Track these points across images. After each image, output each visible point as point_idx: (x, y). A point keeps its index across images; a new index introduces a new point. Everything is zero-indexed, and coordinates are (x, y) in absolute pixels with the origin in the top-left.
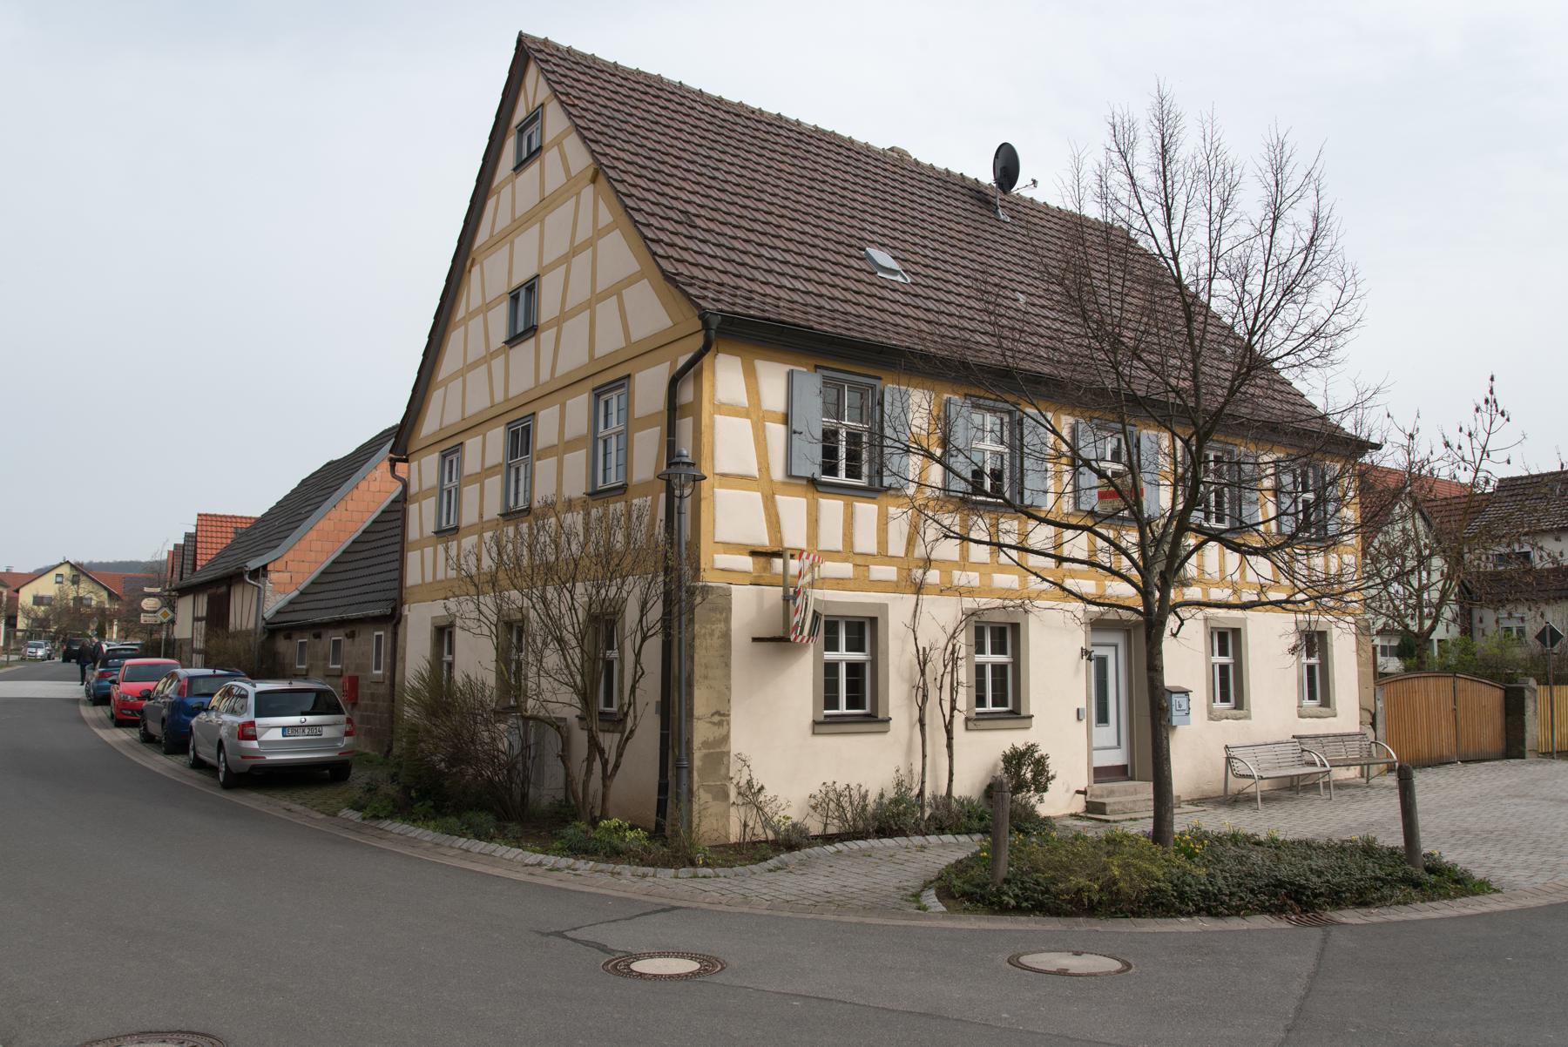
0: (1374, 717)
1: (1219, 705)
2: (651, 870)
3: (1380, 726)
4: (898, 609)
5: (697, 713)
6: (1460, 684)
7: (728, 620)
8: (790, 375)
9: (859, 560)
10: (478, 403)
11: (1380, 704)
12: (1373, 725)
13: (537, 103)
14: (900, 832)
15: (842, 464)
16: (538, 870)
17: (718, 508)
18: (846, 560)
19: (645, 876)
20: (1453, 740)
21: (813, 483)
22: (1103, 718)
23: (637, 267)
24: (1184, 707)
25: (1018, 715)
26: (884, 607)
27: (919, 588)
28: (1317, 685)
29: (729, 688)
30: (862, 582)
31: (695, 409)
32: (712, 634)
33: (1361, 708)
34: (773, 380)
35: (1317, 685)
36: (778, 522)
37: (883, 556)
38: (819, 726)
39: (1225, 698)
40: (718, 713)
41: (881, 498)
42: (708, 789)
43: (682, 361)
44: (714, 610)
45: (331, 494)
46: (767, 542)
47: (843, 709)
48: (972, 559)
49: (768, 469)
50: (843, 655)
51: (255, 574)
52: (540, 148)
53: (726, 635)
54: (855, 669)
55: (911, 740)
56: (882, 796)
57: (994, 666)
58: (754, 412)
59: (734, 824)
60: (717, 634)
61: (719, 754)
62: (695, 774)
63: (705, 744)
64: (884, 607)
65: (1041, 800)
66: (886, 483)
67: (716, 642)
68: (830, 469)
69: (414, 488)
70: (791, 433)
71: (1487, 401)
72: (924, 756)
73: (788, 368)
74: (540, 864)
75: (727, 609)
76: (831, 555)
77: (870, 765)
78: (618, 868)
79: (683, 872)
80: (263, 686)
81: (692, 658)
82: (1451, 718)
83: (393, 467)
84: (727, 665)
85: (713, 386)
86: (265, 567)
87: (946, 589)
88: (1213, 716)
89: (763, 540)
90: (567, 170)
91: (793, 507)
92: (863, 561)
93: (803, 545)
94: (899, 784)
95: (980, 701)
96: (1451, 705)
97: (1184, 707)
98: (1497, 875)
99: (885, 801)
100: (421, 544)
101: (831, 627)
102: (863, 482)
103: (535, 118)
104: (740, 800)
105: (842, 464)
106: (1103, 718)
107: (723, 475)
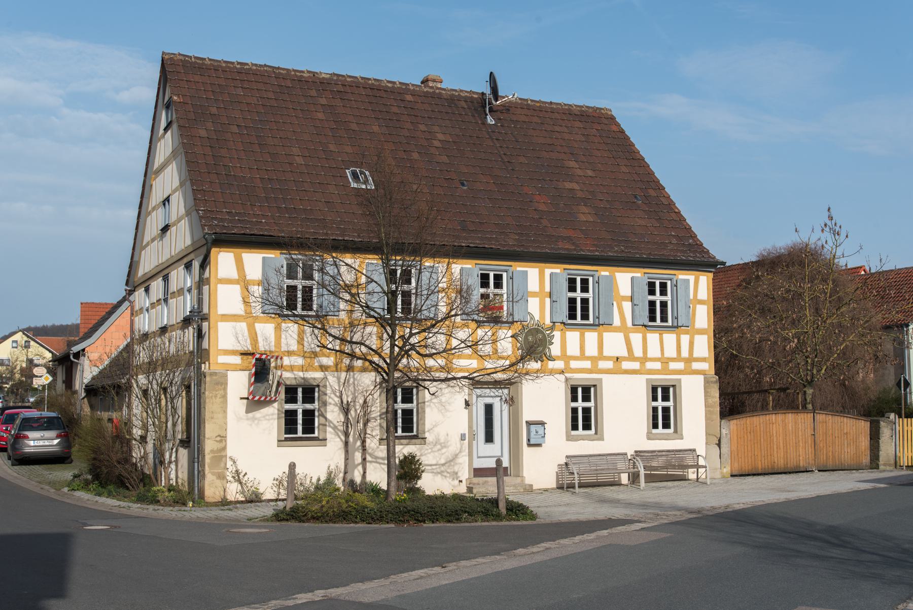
0: (719, 441)
4: (332, 381)
7: (225, 389)
8: (264, 258)
11: (724, 431)
12: (719, 445)
20: (810, 450)
22: (489, 438)
24: (541, 432)
25: (418, 438)
26: (601, 380)
27: (350, 369)
28: (663, 418)
29: (226, 424)
30: (665, 370)
31: (208, 281)
32: (216, 397)
33: (707, 434)
34: (254, 262)
35: (663, 418)
37: (583, 357)
40: (219, 436)
42: (213, 474)
51: (77, 355)
56: (319, 480)
57: (404, 411)
58: (244, 283)
61: (220, 455)
63: (212, 451)
64: (601, 380)
76: (673, 360)
77: (318, 462)
84: (225, 412)
86: (83, 350)
89: (250, 348)
91: (266, 330)
92: (665, 361)
94: (330, 474)
96: (810, 432)
106: (489, 438)
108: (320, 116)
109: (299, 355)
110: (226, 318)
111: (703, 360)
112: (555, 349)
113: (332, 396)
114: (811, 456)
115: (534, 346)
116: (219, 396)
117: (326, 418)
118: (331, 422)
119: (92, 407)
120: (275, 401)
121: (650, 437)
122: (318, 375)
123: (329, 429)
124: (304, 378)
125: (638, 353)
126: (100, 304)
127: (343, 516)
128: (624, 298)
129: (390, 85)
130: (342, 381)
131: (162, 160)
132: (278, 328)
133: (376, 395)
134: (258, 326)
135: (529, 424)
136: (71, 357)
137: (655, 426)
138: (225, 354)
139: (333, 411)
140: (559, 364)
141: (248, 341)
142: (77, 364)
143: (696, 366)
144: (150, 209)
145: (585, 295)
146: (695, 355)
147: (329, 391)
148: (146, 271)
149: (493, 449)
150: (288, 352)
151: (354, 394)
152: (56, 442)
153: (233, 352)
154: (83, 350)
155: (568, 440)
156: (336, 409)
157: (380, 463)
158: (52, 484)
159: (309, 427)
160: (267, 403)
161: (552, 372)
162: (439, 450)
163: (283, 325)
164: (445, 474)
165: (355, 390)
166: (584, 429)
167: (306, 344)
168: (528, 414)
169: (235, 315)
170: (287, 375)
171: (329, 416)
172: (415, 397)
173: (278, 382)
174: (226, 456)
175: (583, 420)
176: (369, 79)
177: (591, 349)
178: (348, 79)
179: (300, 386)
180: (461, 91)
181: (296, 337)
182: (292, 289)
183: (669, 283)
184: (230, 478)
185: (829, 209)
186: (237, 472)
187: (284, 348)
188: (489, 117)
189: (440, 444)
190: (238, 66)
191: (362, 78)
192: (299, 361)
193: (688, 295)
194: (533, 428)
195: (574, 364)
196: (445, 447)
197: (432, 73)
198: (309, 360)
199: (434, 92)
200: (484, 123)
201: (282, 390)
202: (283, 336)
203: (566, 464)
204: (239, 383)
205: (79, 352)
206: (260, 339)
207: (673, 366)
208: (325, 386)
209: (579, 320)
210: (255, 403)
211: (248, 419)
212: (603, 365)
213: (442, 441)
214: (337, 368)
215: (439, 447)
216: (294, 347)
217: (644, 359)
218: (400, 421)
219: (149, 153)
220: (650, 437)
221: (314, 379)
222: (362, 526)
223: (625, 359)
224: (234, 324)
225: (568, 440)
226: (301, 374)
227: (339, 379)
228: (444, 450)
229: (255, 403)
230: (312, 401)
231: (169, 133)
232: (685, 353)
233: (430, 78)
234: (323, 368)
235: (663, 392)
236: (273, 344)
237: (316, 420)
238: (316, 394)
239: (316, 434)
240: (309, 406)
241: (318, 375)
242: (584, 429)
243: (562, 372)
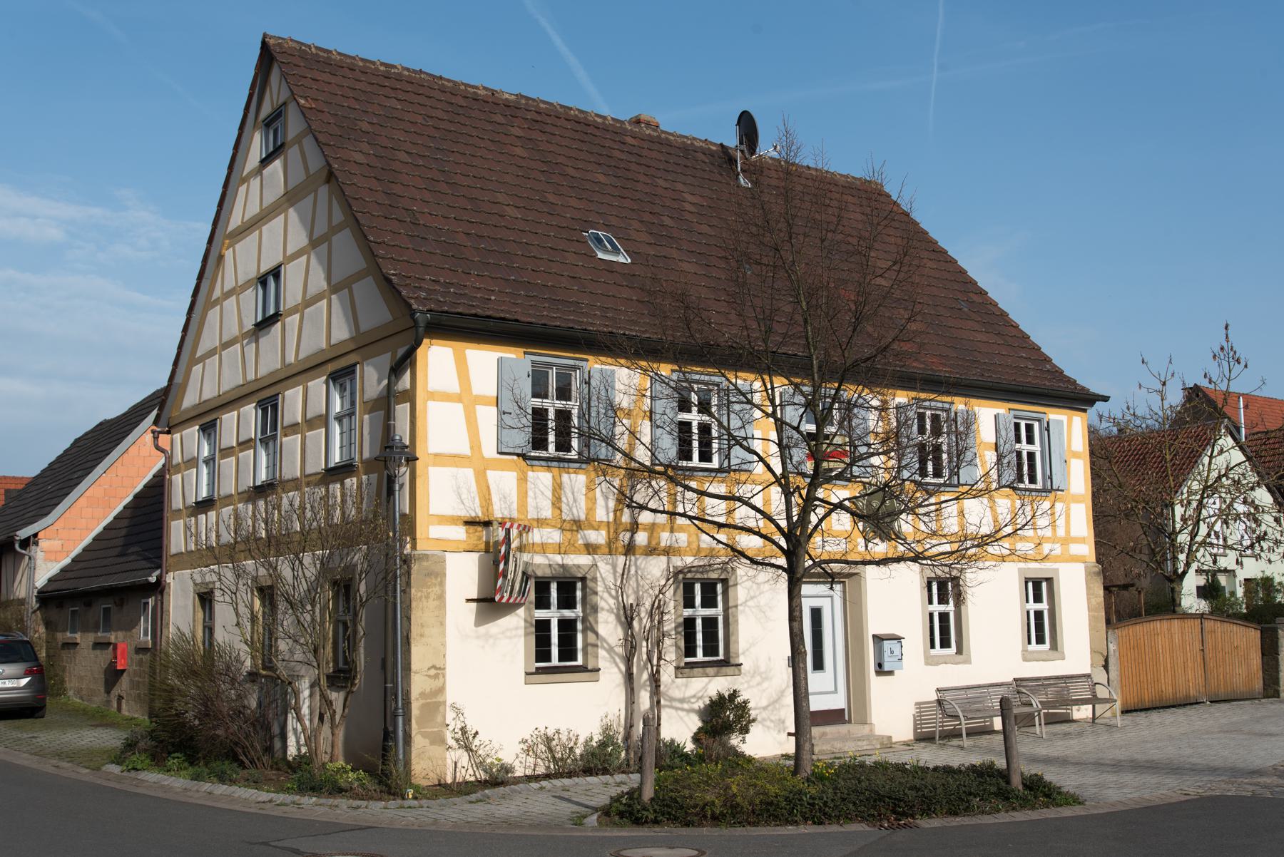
0: (1106, 660)
1: (1034, 646)
2: (364, 803)
3: (1112, 667)
4: (606, 571)
5: (414, 667)
8: (500, 360)
10: (232, 379)
11: (1112, 647)
12: (1106, 667)
13: (280, 102)
14: (605, 771)
15: (552, 437)
16: (268, 806)
19: (358, 807)
21: (524, 456)
23: (365, 265)
24: (897, 652)
25: (727, 664)
26: (1057, 570)
27: (630, 549)
28: (1041, 629)
29: (444, 645)
32: (427, 597)
34: (485, 362)
35: (1041, 629)
39: (945, 643)
40: (434, 667)
42: (425, 735)
43: (401, 352)
45: (95, 466)
46: (480, 515)
47: (700, 656)
49: (480, 447)
50: (701, 612)
51: (26, 543)
52: (283, 145)
54: (567, 627)
57: (705, 620)
58: (466, 398)
59: (456, 765)
61: (435, 704)
62: (413, 721)
63: (422, 695)
65: (744, 741)
68: (539, 443)
69: (178, 458)
71: (1222, 349)
74: (270, 801)
77: (586, 708)
78: (336, 802)
79: (392, 804)
80: (575, 412)
81: (409, 619)
82: (1199, 659)
83: (156, 438)
84: (442, 624)
86: (36, 535)
87: (652, 551)
88: (930, 661)
89: (477, 512)
90: (306, 168)
91: (504, 482)
95: (690, 651)
96: (1198, 646)
97: (897, 652)
98: (1087, 793)
100: (177, 514)
101: (542, 587)
102: (715, 464)
103: (279, 115)
105: (552, 437)
107: (436, 455)
108: (519, 151)
109: (554, 527)
110: (444, 459)
111: (1081, 540)
113: (606, 595)
114: (1201, 681)
116: (432, 596)
117: (597, 634)
118: (604, 640)
119: (48, 624)
120: (518, 606)
121: (1027, 657)
122: (584, 560)
123: (602, 653)
124: (563, 566)
126: (14, 478)
127: (818, 813)
128: (483, 400)
129: (599, 120)
130: (620, 570)
131: (254, 209)
132: (523, 480)
133: (670, 593)
134: (492, 475)
135: (878, 639)
136: (17, 546)
137: (933, 646)
138: (439, 524)
139: (607, 622)
141: (477, 500)
142: (24, 555)
144: (217, 293)
147: (600, 589)
148: (206, 396)
150: (538, 520)
151: (636, 592)
152: (24, 681)
153: (453, 520)
154: (36, 535)
155: (927, 664)
156: (612, 618)
157: (677, 709)
158: (40, 753)
159: (568, 651)
160: (509, 608)
162: (759, 684)
163: (530, 474)
164: (768, 723)
165: (638, 585)
166: (1038, 643)
167: (564, 507)
168: (875, 624)
169: (455, 456)
170: (539, 560)
171: (601, 629)
172: (720, 598)
173: (524, 573)
174: (445, 703)
175: (945, 633)
176: (571, 109)
178: (542, 105)
179: (553, 578)
180: (694, 139)
181: (549, 494)
182: (539, 414)
183: (1036, 425)
184: (452, 742)
185: (1226, 328)
186: (464, 730)
187: (532, 514)
188: (741, 177)
189: (760, 674)
190: (382, 68)
191: (562, 106)
192: (554, 536)
193: (1062, 444)
194: (887, 644)
196: (766, 679)
198: (568, 534)
199: (659, 137)
200: (739, 186)
201: (531, 584)
202: (530, 493)
203: (939, 702)
204: (462, 575)
205: (29, 538)
206: (495, 498)
208: (595, 580)
210: (490, 604)
211: (478, 637)
213: (762, 669)
214: (610, 549)
215: (758, 679)
216: (547, 512)
218: (699, 637)
219: (220, 205)
220: (1027, 657)
221: (578, 566)
222: (807, 829)
224: (454, 470)
226: (558, 559)
227: (614, 567)
228: (765, 685)
229: (490, 604)
231: (277, 164)
233: (642, 118)
234: (590, 549)
235: (1039, 587)
236: (515, 506)
237: (580, 637)
238: (579, 594)
239: (580, 662)
240: (568, 614)
241: (584, 560)
242: (1038, 643)
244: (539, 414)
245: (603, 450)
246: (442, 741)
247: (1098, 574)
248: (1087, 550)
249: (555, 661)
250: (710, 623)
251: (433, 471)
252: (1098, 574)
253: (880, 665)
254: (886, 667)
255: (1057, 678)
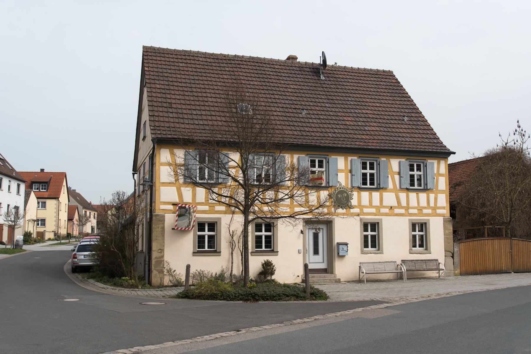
0: (453, 254)
4: (225, 219)
6: (515, 242)
7: (164, 224)
8: (400, 162)
9: (211, 205)
11: (456, 249)
12: (453, 257)
17: (161, 192)
18: (206, 205)
21: (408, 189)
22: (316, 252)
26: (429, 220)
29: (164, 243)
32: (158, 228)
36: (182, 195)
37: (371, 206)
38: (195, 253)
39: (421, 246)
40: (160, 249)
41: (427, 192)
42: (157, 270)
44: (159, 221)
48: (384, 205)
50: (370, 233)
53: (163, 228)
55: (229, 258)
56: (216, 274)
60: (160, 227)
61: (161, 260)
63: (156, 258)
64: (429, 220)
66: (220, 182)
67: (160, 230)
70: (400, 177)
72: (232, 263)
73: (398, 160)
75: (163, 221)
76: (425, 208)
84: (163, 236)
85: (160, 158)
89: (176, 200)
91: (403, 196)
92: (420, 209)
93: (191, 202)
99: (217, 276)
102: (422, 188)
104: (168, 274)
106: (316, 252)
111: (444, 208)
112: (354, 202)
115: (342, 200)
125: (404, 203)
140: (356, 210)
143: (439, 211)
145: (372, 171)
146: (438, 205)
149: (319, 258)
161: (353, 215)
168: (338, 238)
177: (376, 202)
185: (518, 122)
194: (341, 246)
195: (366, 210)
197: (293, 54)
207: (425, 211)
209: (416, 187)
210: (179, 231)
212: (383, 210)
217: (407, 208)
223: (396, 207)
225: (362, 253)
230: (213, 230)
232: (432, 204)
243: (358, 215)
244: (364, 175)
245: (230, 181)
246: (163, 272)
247: (450, 221)
248: (446, 212)
249: (206, 249)
250: (373, 237)
251: (162, 188)
252: (450, 221)
253: (338, 253)
254: (340, 254)
255: (416, 260)
